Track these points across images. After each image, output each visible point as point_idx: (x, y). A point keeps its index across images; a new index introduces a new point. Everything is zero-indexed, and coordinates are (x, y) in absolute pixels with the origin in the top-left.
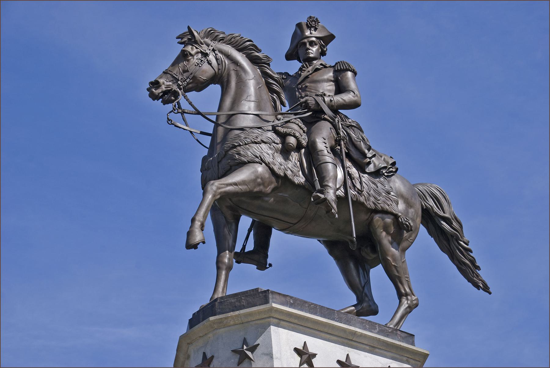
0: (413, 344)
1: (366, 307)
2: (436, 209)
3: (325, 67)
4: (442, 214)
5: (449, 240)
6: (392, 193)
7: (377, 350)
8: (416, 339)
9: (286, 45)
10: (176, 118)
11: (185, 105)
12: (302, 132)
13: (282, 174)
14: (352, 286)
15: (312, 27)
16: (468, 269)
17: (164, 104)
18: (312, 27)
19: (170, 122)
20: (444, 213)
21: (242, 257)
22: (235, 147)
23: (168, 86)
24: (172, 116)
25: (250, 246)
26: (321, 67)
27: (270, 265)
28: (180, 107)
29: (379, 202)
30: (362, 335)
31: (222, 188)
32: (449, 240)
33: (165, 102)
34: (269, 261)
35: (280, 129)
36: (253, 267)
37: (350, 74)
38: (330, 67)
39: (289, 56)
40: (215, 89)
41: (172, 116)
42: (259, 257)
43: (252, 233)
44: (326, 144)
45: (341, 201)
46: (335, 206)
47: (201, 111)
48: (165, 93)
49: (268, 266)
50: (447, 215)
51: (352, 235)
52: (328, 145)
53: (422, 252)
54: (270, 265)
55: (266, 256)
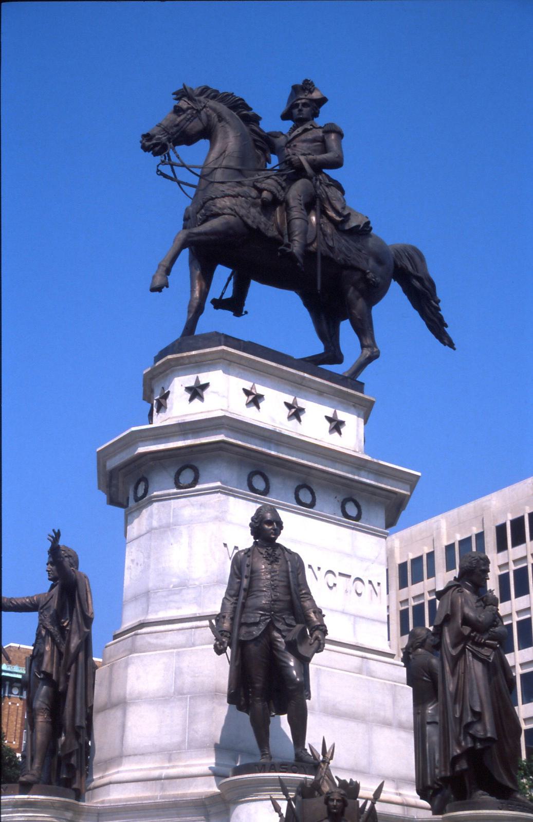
0: (362, 392)
1: (333, 355)
2: (410, 268)
3: (314, 127)
4: (416, 273)
5: (424, 298)
6: (363, 252)
7: (204, 363)
8: (366, 388)
9: (283, 107)
10: (166, 169)
11: (174, 159)
12: (279, 188)
13: (255, 227)
14: (322, 336)
15: (306, 89)
16: (437, 326)
17: (154, 156)
18: (306, 89)
19: (159, 173)
20: (418, 273)
21: (219, 304)
22: (212, 199)
23: (159, 139)
24: (161, 168)
25: (229, 294)
26: (312, 127)
27: (246, 313)
28: (169, 159)
29: (350, 259)
30: (310, 380)
31: (193, 237)
32: (424, 298)
33: (155, 154)
34: (245, 309)
35: (259, 185)
36: (229, 314)
37: (333, 136)
38: (320, 128)
39: (286, 116)
40: (204, 144)
41: (161, 168)
42: (235, 305)
43: (232, 282)
44: (300, 200)
45: (309, 255)
46: (301, 260)
47: (187, 163)
48: (155, 145)
49: (243, 313)
50: (419, 275)
51: (316, 285)
52: (302, 202)
53: (393, 309)
54: (246, 313)
55: (243, 305)
